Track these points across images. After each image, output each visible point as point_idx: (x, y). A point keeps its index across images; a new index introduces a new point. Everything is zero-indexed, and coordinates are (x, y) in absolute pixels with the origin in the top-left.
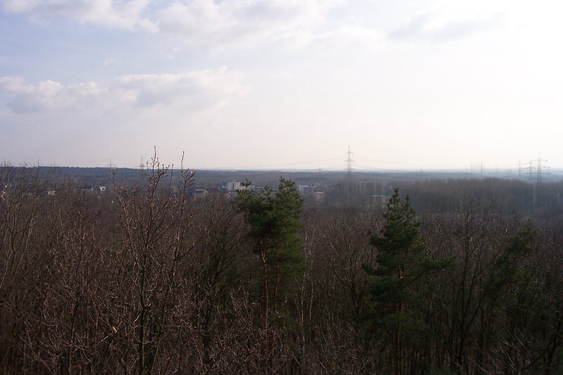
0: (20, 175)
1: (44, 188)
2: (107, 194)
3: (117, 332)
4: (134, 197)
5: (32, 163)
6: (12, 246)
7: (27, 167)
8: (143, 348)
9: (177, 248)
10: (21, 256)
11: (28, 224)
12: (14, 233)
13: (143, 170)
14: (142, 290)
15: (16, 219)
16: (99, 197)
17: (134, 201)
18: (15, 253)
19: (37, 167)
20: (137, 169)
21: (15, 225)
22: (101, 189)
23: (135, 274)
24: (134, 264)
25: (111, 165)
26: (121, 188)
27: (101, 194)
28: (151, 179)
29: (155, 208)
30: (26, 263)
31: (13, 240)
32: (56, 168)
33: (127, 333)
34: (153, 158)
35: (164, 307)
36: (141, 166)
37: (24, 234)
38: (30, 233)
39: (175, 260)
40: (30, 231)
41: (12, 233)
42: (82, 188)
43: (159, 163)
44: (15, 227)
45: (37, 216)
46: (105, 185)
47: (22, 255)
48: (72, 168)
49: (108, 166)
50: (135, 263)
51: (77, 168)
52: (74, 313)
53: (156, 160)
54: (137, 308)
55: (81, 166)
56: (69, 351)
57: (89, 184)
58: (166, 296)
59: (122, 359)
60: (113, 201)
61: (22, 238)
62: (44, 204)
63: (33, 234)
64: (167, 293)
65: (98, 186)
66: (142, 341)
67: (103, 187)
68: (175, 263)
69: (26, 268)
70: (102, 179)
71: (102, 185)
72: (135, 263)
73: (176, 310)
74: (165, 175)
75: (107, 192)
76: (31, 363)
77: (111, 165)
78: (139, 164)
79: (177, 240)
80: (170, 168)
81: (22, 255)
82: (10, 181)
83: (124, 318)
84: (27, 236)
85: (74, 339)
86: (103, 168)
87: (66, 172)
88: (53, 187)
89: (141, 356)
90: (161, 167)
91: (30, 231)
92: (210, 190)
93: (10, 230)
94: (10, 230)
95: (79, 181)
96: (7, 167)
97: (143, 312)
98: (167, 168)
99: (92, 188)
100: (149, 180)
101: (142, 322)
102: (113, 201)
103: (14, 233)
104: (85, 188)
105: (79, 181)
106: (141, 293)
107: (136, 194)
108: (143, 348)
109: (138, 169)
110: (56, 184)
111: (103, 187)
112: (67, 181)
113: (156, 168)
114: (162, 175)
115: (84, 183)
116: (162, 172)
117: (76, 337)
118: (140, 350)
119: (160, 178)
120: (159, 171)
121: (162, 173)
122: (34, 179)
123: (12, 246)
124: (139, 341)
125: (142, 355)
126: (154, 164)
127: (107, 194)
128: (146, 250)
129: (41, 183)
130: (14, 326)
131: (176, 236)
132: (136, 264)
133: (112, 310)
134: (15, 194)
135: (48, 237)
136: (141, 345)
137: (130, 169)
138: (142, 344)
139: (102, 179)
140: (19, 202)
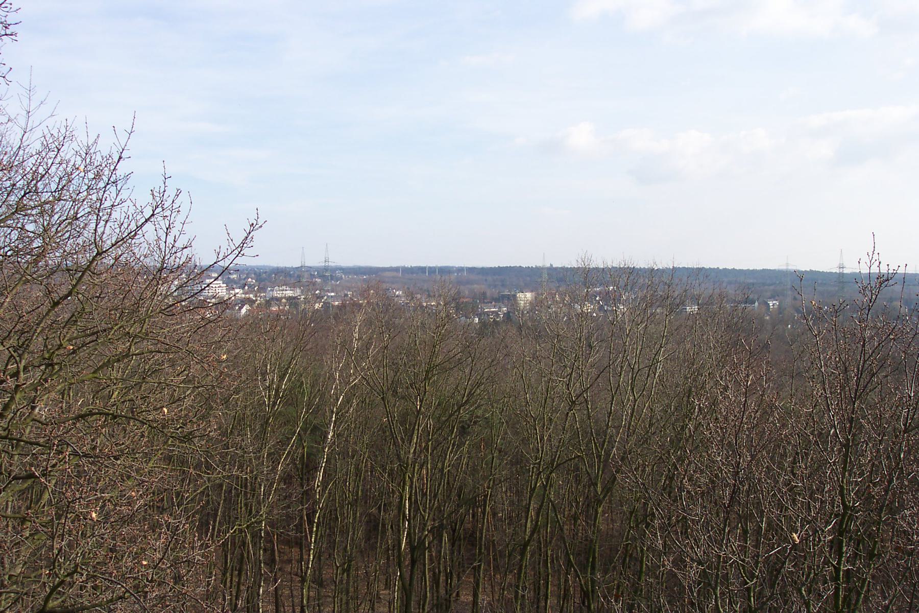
0: (647, 281)
1: (682, 302)
2: (780, 313)
3: (800, 542)
4: (834, 319)
5: (664, 261)
6: (632, 389)
7: (656, 268)
8: (841, 576)
9: (909, 411)
10: (645, 406)
11: (657, 357)
12: (636, 370)
13: (842, 275)
14: (843, 477)
15: (639, 348)
16: (768, 318)
17: (835, 325)
18: (635, 401)
19: (671, 267)
20: (832, 273)
21: (637, 358)
22: (771, 305)
23: (832, 449)
24: (831, 433)
25: (787, 264)
26: (812, 303)
27: (770, 312)
28: (864, 289)
29: (872, 338)
30: (651, 417)
31: (633, 379)
32: (700, 270)
33: (814, 545)
34: (870, 254)
35: (881, 510)
36: (840, 268)
37: (650, 372)
38: (658, 371)
39: (905, 432)
40: (659, 368)
41: (633, 369)
42: (740, 302)
43: (880, 263)
44: (637, 360)
45: (669, 346)
46: (777, 298)
47: (647, 405)
48: (725, 269)
49: (783, 268)
50: (833, 430)
51: (731, 269)
52: (730, 503)
53: (876, 256)
54: (833, 507)
55: (738, 267)
56: (719, 562)
57: (751, 297)
58: (886, 491)
59: (803, 589)
60: (789, 326)
61: (647, 379)
62: (681, 325)
63: (663, 374)
64: (889, 486)
65: (766, 300)
66: (839, 563)
67: (774, 302)
68: (905, 435)
69: (651, 425)
70: (772, 288)
71: (773, 297)
72: (833, 430)
73: (903, 518)
74: (891, 282)
75: (780, 309)
76: (660, 571)
77: (787, 264)
78: (837, 265)
79: (910, 397)
80: (901, 271)
81: (647, 405)
82: (631, 289)
83: (812, 520)
84: (655, 375)
85: (727, 544)
86: (775, 270)
87: (717, 277)
88: (696, 300)
89: (837, 589)
90: (884, 270)
91: (659, 368)
92: (705, 304)
93: (629, 365)
94: (629, 365)
95: (736, 291)
96: (628, 268)
97: (844, 515)
98: (895, 272)
99: (756, 304)
100: (862, 291)
101: (840, 530)
102: (789, 326)
103: (636, 370)
104: (746, 303)
105: (736, 291)
106: (842, 481)
107: (838, 314)
108: (841, 576)
109: (834, 272)
110: (699, 296)
111: (774, 302)
112: (717, 291)
113: (875, 270)
114: (886, 283)
115: (744, 294)
116: (885, 278)
117: (730, 542)
118: (836, 579)
119: (881, 288)
120: (880, 276)
121: (884, 280)
122: (667, 287)
123: (632, 389)
124: (835, 563)
125: (840, 589)
126: (872, 263)
127: (780, 313)
128: (854, 409)
129: (676, 293)
130: (631, 513)
131: (908, 389)
132: (835, 433)
133: (791, 505)
134: (639, 309)
135: (686, 378)
136: (837, 570)
137: (819, 272)
138: (840, 568)
139: (772, 288)
140: (644, 322)
